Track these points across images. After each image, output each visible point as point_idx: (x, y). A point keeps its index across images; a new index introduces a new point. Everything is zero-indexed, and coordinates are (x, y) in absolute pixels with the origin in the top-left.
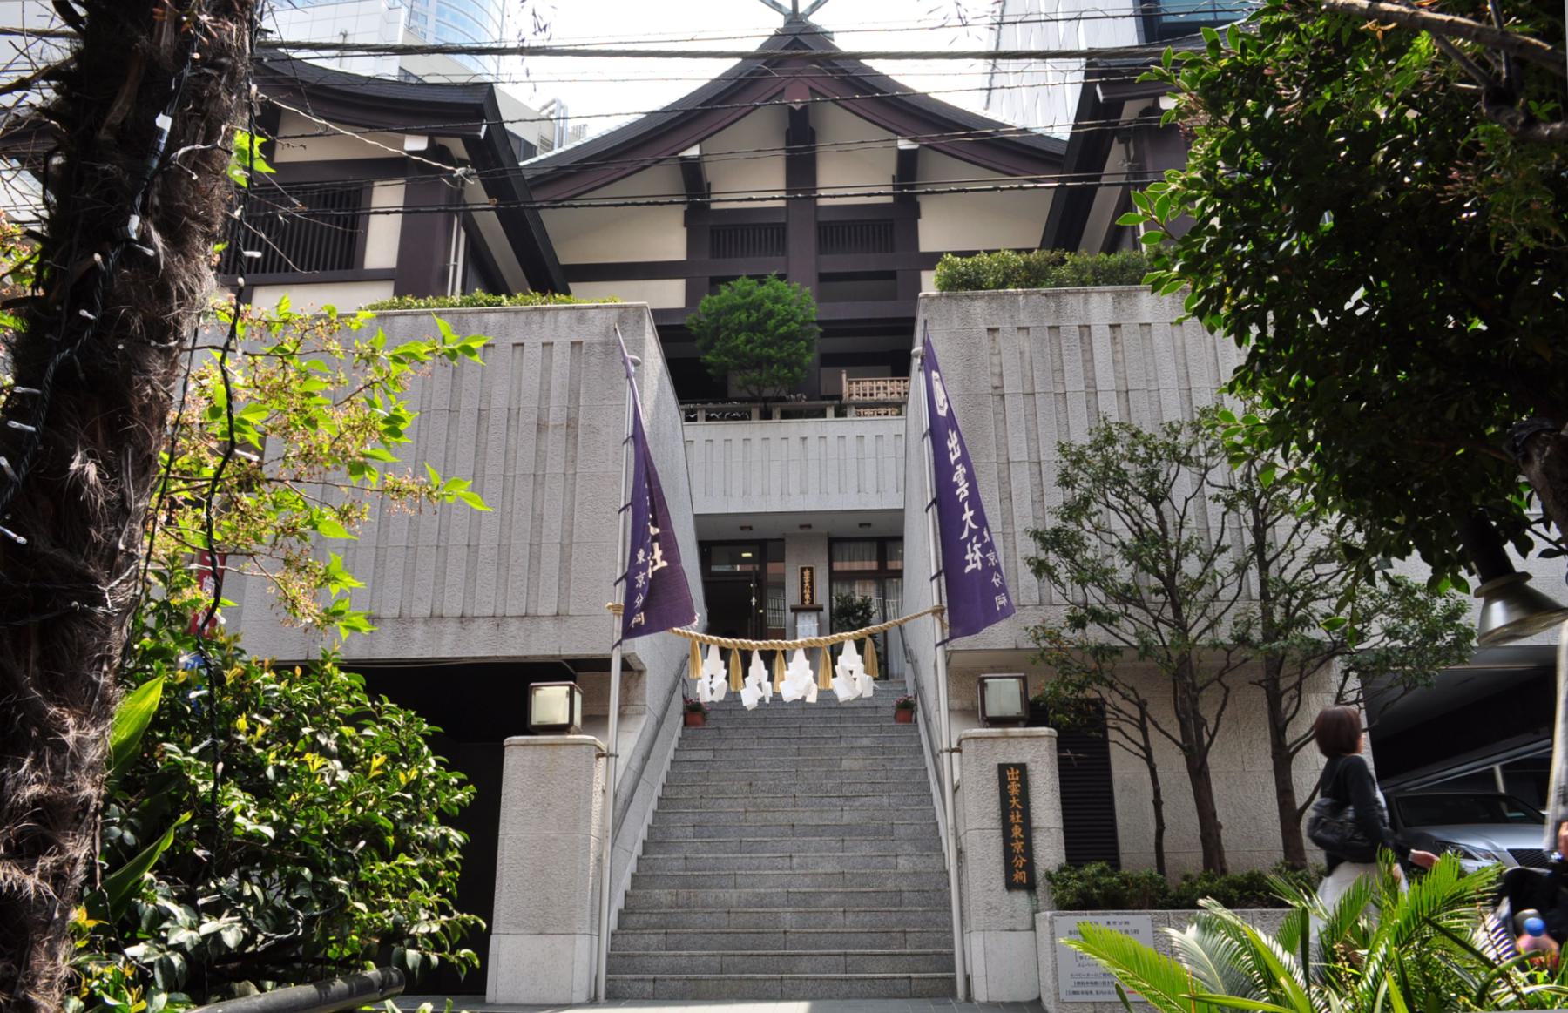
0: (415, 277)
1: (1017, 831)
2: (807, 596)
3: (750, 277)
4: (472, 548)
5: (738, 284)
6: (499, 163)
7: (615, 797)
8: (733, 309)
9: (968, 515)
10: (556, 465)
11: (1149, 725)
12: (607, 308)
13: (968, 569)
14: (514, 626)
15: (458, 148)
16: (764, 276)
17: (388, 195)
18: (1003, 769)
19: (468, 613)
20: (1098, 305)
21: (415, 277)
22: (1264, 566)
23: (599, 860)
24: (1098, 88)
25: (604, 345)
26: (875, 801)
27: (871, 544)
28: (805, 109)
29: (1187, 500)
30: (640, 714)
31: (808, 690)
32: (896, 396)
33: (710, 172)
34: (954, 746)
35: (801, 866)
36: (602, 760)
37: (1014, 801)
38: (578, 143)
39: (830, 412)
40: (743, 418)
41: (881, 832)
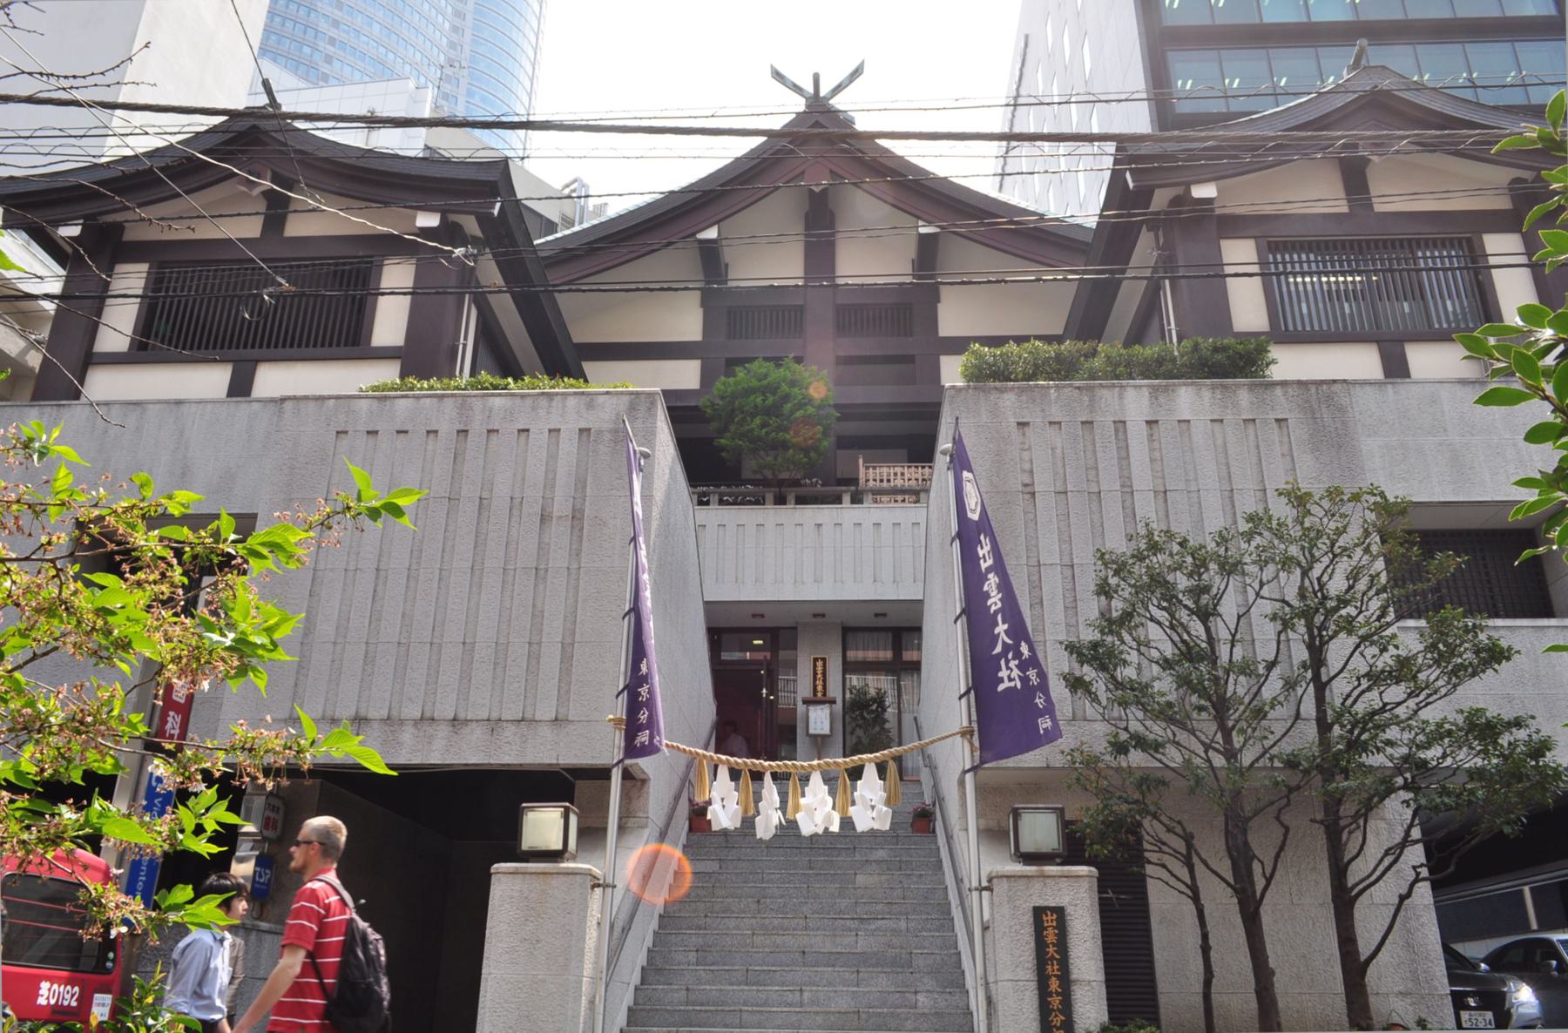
0: (423, 357)
1: (1054, 985)
2: (820, 688)
3: (766, 359)
4: (468, 646)
5: (754, 366)
6: (514, 243)
7: (612, 927)
8: (748, 392)
9: (1001, 628)
10: (559, 559)
11: (1195, 860)
12: (617, 393)
13: (1001, 688)
14: (509, 731)
15: (471, 225)
16: (781, 359)
17: (397, 274)
18: (1039, 912)
19: (462, 716)
20: (1135, 400)
21: (423, 357)
22: (1321, 688)
23: (592, 1002)
24: (1128, 176)
25: (626, 407)
26: (892, 924)
27: (891, 635)
28: (824, 191)
29: (1239, 617)
30: (646, 826)
31: (828, 818)
32: (913, 482)
33: (728, 254)
34: (984, 884)
35: (813, 1002)
36: (598, 891)
37: (1051, 950)
38: (595, 222)
39: (846, 498)
40: (757, 503)
41: (901, 964)
